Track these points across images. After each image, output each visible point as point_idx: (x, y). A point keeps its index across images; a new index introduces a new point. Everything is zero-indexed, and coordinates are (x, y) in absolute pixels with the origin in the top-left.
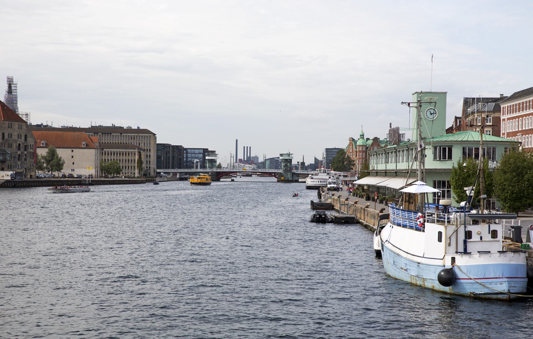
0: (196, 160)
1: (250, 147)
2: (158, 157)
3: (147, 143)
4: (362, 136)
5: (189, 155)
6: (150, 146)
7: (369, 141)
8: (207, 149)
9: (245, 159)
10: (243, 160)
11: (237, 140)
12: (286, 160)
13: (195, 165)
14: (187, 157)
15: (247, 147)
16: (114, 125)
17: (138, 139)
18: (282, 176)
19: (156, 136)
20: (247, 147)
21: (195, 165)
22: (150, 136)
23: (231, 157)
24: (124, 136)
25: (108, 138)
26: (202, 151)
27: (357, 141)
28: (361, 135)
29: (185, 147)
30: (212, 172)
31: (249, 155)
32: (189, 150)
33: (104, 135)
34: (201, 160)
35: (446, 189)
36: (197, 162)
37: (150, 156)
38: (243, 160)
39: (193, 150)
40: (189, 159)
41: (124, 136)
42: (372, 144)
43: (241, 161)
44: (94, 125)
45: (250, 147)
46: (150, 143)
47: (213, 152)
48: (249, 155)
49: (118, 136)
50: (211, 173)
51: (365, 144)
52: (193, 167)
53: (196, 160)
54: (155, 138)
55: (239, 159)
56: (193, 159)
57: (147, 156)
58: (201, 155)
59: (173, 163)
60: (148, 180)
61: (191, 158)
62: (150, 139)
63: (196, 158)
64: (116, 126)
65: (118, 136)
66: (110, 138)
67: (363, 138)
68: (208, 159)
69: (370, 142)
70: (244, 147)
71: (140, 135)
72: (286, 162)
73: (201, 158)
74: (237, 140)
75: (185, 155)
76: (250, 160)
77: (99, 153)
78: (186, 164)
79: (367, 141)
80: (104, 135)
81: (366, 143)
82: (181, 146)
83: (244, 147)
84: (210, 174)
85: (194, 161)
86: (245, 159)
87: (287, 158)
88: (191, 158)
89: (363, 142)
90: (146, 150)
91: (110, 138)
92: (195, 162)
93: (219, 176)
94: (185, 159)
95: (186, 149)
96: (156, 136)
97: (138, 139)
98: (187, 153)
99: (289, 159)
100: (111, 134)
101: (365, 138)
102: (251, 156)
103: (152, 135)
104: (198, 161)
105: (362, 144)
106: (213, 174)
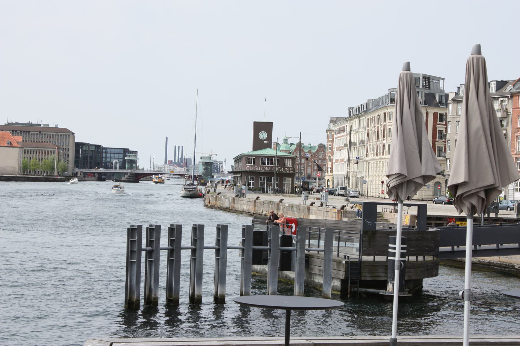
0: (114, 161)
1: (182, 147)
2: (77, 157)
3: (66, 142)
4: (286, 141)
5: (108, 155)
6: (68, 146)
7: (293, 146)
8: (128, 149)
9: (176, 161)
10: (173, 162)
11: (167, 138)
12: (206, 163)
13: (114, 166)
14: (106, 158)
15: (179, 147)
16: (31, 123)
17: (57, 138)
18: (202, 179)
19: (75, 135)
20: (179, 147)
21: (114, 166)
22: (69, 136)
23: (151, 158)
24: (42, 134)
25: (29, 136)
26: (122, 152)
27: (281, 145)
28: (284, 140)
29: (104, 147)
30: (131, 174)
31: (180, 156)
32: (109, 150)
33: (25, 134)
34: (121, 160)
35: (251, 181)
36: (116, 163)
37: (68, 155)
38: (173, 162)
39: (112, 150)
40: (108, 160)
41: (42, 134)
42: (296, 150)
43: (171, 162)
44: (10, 122)
45: (182, 147)
46: (69, 142)
47: (135, 152)
48: (180, 156)
49: (37, 134)
50: (130, 174)
51: (288, 149)
52: (111, 168)
53: (114, 161)
54: (74, 137)
55: (169, 161)
56: (112, 160)
57: (66, 155)
58: (121, 156)
59: (91, 162)
60: (67, 179)
61: (110, 158)
62: (69, 138)
63: (115, 158)
64: (33, 123)
65: (37, 134)
66: (29, 136)
67: (287, 143)
68: (128, 160)
69: (294, 147)
70: (175, 146)
71: (59, 133)
72: (206, 165)
73: (121, 158)
74: (167, 138)
75: (104, 155)
76: (182, 162)
77: (22, 151)
78: (105, 164)
79: (291, 146)
80: (25, 134)
81: (289, 148)
82: (100, 145)
83: (175, 146)
84: (129, 175)
85: (113, 161)
86: (176, 161)
87: (208, 161)
88: (110, 158)
89: (286, 147)
90: (64, 149)
91: (29, 136)
92: (114, 162)
93: (138, 178)
94: (104, 159)
95: (105, 148)
96: (75, 135)
97: (57, 138)
98: (106, 153)
99: (210, 162)
100: (29, 132)
101: (289, 142)
102: (183, 157)
103: (71, 134)
104: (117, 161)
105: (285, 149)
106: (132, 175)
